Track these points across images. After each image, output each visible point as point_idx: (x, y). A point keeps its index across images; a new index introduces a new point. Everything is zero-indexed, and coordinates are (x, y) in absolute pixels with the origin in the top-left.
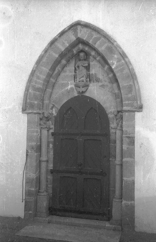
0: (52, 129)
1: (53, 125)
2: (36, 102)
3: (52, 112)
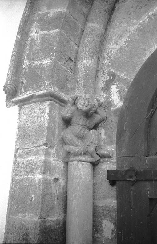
0: (109, 157)
1: (111, 142)
2: (45, 62)
3: (107, 98)
